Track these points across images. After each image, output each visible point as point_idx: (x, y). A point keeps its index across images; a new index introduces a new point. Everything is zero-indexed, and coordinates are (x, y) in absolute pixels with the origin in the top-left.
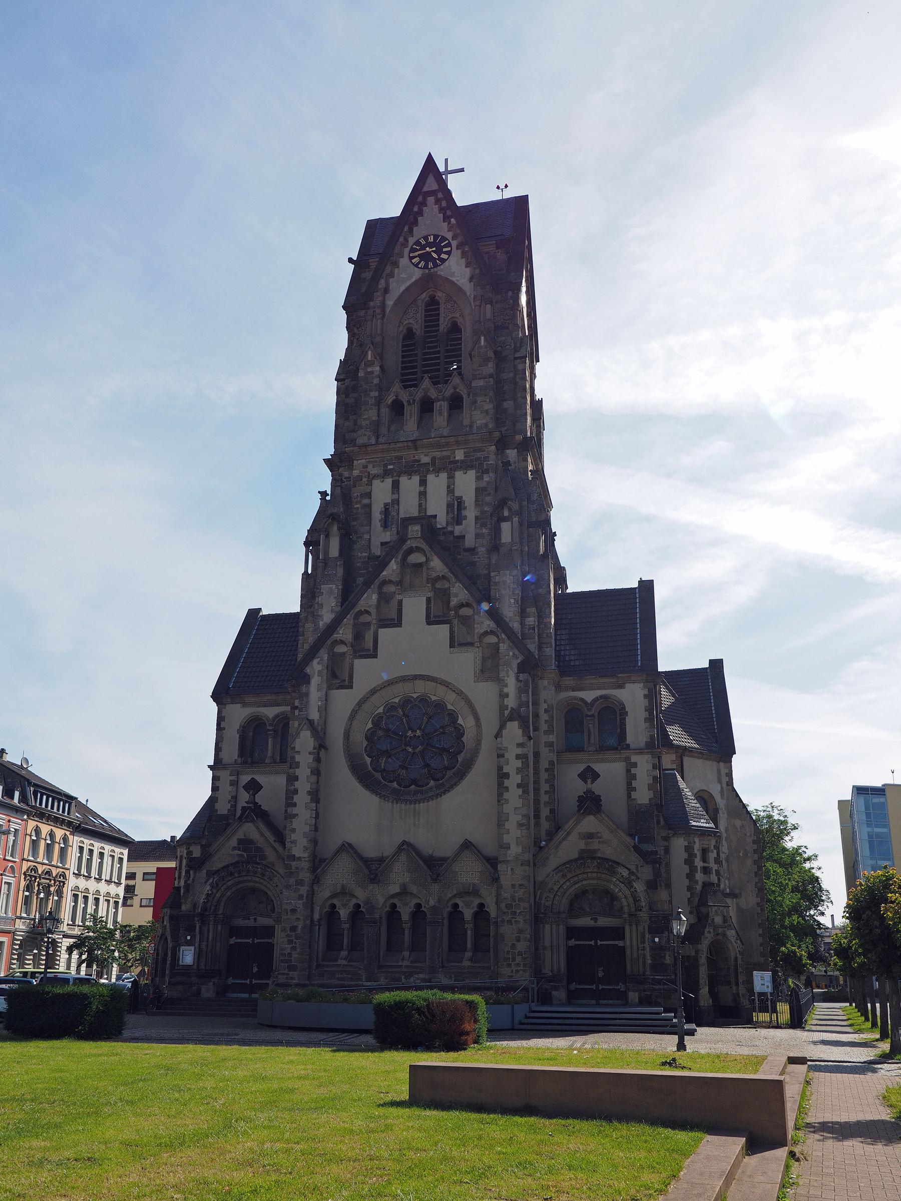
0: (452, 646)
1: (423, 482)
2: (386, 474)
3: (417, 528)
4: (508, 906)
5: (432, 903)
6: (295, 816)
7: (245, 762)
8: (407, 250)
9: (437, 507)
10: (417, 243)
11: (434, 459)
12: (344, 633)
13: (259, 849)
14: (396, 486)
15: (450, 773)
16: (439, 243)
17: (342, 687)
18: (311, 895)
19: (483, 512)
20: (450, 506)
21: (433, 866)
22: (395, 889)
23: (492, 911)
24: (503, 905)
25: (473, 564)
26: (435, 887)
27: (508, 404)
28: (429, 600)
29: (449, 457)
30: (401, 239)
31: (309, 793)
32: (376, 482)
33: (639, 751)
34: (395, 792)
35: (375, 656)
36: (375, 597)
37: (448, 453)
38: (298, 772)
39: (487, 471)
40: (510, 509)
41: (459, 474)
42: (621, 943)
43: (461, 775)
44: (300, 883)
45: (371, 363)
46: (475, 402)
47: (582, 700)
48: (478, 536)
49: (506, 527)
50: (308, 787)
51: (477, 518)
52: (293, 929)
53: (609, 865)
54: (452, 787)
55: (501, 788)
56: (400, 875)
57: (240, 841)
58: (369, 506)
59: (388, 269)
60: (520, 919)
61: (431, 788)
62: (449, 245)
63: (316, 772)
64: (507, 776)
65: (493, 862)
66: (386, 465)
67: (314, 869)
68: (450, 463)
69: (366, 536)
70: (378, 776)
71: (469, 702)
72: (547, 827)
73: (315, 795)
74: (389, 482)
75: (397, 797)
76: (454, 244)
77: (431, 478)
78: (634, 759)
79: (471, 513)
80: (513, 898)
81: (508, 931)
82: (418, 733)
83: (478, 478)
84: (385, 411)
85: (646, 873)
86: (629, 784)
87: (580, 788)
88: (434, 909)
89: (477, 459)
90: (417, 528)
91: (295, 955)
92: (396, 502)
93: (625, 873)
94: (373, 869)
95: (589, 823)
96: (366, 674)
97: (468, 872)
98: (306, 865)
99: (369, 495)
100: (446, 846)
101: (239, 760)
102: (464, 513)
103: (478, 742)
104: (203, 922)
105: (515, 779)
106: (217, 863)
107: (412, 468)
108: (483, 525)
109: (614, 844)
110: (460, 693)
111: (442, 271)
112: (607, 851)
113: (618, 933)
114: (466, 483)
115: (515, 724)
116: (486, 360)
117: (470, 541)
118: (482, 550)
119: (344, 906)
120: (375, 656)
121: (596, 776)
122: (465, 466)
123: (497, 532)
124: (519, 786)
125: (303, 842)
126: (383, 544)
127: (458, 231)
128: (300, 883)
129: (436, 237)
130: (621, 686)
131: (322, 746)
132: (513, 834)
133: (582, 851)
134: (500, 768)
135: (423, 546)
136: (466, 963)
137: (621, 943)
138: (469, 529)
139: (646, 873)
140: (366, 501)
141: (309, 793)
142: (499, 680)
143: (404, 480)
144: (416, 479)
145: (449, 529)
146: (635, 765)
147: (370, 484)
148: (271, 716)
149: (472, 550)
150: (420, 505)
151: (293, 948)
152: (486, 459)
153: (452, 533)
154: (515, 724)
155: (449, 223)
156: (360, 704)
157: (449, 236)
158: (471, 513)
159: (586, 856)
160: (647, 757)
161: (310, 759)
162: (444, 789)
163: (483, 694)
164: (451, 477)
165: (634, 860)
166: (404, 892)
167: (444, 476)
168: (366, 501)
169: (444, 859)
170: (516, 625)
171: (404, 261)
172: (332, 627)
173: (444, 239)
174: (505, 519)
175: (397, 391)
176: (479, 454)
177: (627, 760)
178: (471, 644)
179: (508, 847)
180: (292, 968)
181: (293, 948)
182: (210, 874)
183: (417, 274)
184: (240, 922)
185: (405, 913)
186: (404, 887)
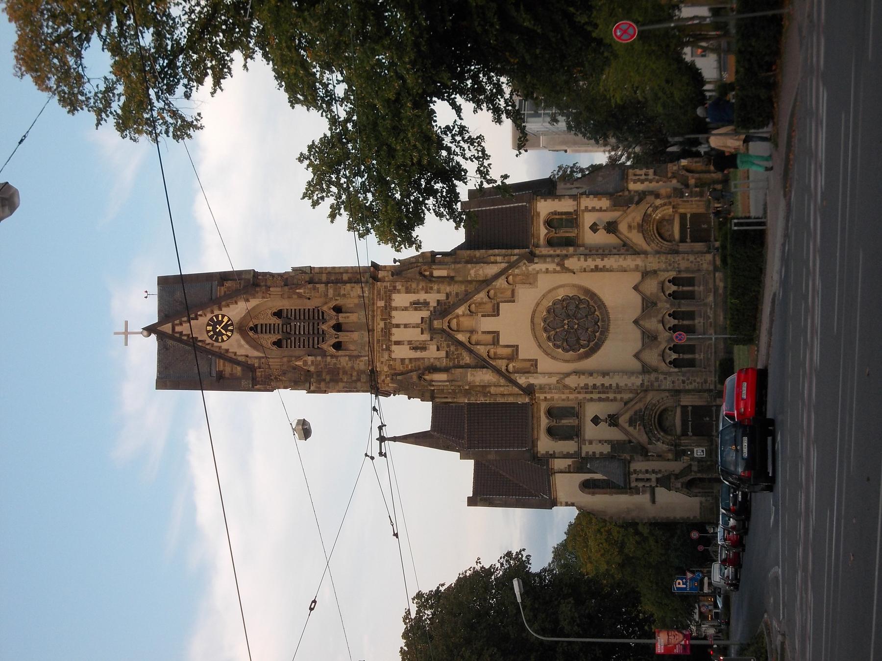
0: (514, 301)
1: (398, 326)
2: (388, 349)
3: (435, 322)
4: (670, 265)
5: (668, 306)
6: (617, 384)
7: (577, 436)
8: (216, 344)
9: (415, 317)
10: (211, 337)
11: (382, 319)
12: (501, 364)
13: (636, 413)
14: (398, 343)
15: (591, 303)
16: (214, 323)
17: (536, 365)
18: (666, 374)
19: (423, 289)
20: (416, 309)
21: (648, 304)
22: (660, 326)
23: (672, 274)
24: (669, 268)
25: (457, 294)
26: (660, 305)
27: (345, 277)
28: (483, 316)
29: (382, 311)
30: (208, 347)
31: (604, 377)
32: (393, 356)
33: (579, 204)
34: (602, 333)
35: (517, 346)
36: (478, 347)
37: (379, 310)
38: (591, 384)
39: (395, 287)
40: (425, 271)
41: (394, 304)
42: (689, 216)
43: (593, 295)
44: (657, 379)
45: (305, 363)
46: (344, 295)
47: (546, 235)
48: (439, 292)
49: (436, 273)
50: (600, 378)
51: (426, 292)
52: (684, 382)
53: (646, 217)
54: (600, 300)
55: (604, 269)
56: (652, 324)
57: (630, 425)
58: (411, 359)
59: (230, 355)
60: (677, 259)
61: (601, 313)
62: (217, 316)
63: (591, 374)
64: (596, 266)
65: (646, 274)
66: (383, 350)
67: (649, 372)
68: (386, 309)
69: (432, 360)
70: (592, 344)
71: (550, 291)
72: (627, 248)
73: (605, 374)
74: (394, 347)
75: (605, 331)
76: (216, 312)
77: (394, 321)
78: (583, 208)
79: (422, 296)
80: (666, 262)
81: (684, 265)
82: (566, 322)
83: (399, 292)
84: (340, 353)
85: (650, 198)
86: (597, 211)
87: (602, 233)
88: (672, 305)
89: (385, 292)
90: (435, 322)
91: (698, 380)
92: (410, 342)
93: (651, 209)
94: (649, 338)
95: (623, 227)
96: (529, 350)
97: (651, 287)
98: (647, 376)
99: (403, 360)
100: (637, 299)
101: (576, 440)
102: (422, 301)
103: (574, 286)
104: (680, 445)
105: (599, 262)
106: (643, 438)
107: (387, 332)
108: (431, 288)
109: (635, 215)
110: (544, 296)
111: (236, 319)
112: (639, 219)
113: (683, 217)
114: (400, 299)
115: (566, 262)
116: (314, 288)
117: (442, 297)
118: (448, 289)
119: (670, 356)
120: (517, 346)
121: (595, 224)
122: (389, 300)
123: (441, 279)
124: (602, 260)
125: (633, 379)
126: (438, 350)
127: (209, 309)
128: (657, 379)
129: (208, 325)
130: (538, 214)
131: (577, 373)
132: (630, 262)
133: (638, 232)
134: (592, 270)
135: (447, 319)
136: (702, 288)
137: (689, 216)
138: (433, 298)
139: (650, 198)
140: (407, 362)
141: (604, 377)
142: (538, 272)
143: (394, 338)
144: (394, 330)
145: (432, 309)
146: (586, 207)
147: (395, 360)
148: (547, 421)
149: (448, 295)
150: (414, 327)
151: (695, 381)
152: (385, 287)
153: (434, 307)
154: (566, 262)
155: (201, 315)
156: (547, 354)
157: (209, 316)
158: (422, 296)
159: (641, 228)
160: (582, 200)
161: (582, 377)
162: (602, 306)
163: (545, 283)
164: (396, 309)
165: (643, 207)
166: (662, 322)
167: (394, 313)
168: (407, 362)
169: (643, 299)
170: (504, 265)
171: (224, 346)
172: (498, 371)
173: (211, 319)
174: (431, 274)
175: (327, 346)
176: (382, 292)
177: (583, 211)
178: (513, 291)
179: (637, 266)
180: (706, 382)
181: (695, 381)
182: (650, 443)
183: (236, 336)
184: (679, 430)
185: (673, 322)
186: (659, 322)
